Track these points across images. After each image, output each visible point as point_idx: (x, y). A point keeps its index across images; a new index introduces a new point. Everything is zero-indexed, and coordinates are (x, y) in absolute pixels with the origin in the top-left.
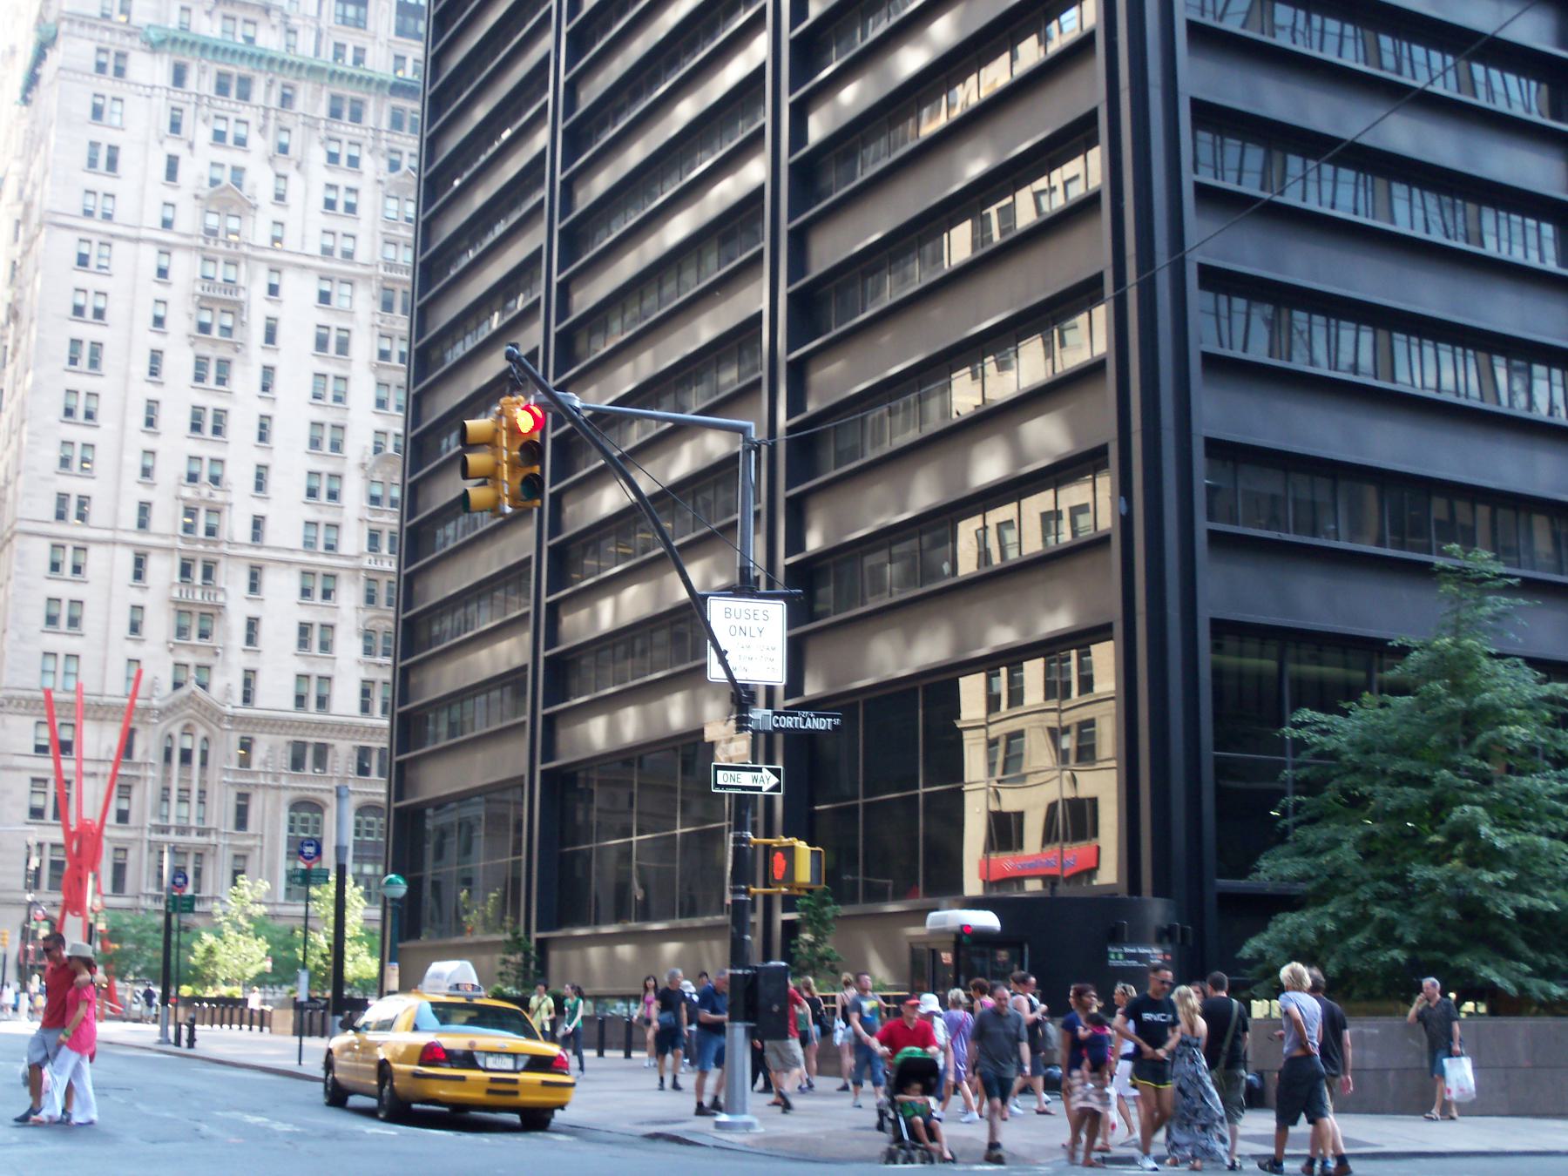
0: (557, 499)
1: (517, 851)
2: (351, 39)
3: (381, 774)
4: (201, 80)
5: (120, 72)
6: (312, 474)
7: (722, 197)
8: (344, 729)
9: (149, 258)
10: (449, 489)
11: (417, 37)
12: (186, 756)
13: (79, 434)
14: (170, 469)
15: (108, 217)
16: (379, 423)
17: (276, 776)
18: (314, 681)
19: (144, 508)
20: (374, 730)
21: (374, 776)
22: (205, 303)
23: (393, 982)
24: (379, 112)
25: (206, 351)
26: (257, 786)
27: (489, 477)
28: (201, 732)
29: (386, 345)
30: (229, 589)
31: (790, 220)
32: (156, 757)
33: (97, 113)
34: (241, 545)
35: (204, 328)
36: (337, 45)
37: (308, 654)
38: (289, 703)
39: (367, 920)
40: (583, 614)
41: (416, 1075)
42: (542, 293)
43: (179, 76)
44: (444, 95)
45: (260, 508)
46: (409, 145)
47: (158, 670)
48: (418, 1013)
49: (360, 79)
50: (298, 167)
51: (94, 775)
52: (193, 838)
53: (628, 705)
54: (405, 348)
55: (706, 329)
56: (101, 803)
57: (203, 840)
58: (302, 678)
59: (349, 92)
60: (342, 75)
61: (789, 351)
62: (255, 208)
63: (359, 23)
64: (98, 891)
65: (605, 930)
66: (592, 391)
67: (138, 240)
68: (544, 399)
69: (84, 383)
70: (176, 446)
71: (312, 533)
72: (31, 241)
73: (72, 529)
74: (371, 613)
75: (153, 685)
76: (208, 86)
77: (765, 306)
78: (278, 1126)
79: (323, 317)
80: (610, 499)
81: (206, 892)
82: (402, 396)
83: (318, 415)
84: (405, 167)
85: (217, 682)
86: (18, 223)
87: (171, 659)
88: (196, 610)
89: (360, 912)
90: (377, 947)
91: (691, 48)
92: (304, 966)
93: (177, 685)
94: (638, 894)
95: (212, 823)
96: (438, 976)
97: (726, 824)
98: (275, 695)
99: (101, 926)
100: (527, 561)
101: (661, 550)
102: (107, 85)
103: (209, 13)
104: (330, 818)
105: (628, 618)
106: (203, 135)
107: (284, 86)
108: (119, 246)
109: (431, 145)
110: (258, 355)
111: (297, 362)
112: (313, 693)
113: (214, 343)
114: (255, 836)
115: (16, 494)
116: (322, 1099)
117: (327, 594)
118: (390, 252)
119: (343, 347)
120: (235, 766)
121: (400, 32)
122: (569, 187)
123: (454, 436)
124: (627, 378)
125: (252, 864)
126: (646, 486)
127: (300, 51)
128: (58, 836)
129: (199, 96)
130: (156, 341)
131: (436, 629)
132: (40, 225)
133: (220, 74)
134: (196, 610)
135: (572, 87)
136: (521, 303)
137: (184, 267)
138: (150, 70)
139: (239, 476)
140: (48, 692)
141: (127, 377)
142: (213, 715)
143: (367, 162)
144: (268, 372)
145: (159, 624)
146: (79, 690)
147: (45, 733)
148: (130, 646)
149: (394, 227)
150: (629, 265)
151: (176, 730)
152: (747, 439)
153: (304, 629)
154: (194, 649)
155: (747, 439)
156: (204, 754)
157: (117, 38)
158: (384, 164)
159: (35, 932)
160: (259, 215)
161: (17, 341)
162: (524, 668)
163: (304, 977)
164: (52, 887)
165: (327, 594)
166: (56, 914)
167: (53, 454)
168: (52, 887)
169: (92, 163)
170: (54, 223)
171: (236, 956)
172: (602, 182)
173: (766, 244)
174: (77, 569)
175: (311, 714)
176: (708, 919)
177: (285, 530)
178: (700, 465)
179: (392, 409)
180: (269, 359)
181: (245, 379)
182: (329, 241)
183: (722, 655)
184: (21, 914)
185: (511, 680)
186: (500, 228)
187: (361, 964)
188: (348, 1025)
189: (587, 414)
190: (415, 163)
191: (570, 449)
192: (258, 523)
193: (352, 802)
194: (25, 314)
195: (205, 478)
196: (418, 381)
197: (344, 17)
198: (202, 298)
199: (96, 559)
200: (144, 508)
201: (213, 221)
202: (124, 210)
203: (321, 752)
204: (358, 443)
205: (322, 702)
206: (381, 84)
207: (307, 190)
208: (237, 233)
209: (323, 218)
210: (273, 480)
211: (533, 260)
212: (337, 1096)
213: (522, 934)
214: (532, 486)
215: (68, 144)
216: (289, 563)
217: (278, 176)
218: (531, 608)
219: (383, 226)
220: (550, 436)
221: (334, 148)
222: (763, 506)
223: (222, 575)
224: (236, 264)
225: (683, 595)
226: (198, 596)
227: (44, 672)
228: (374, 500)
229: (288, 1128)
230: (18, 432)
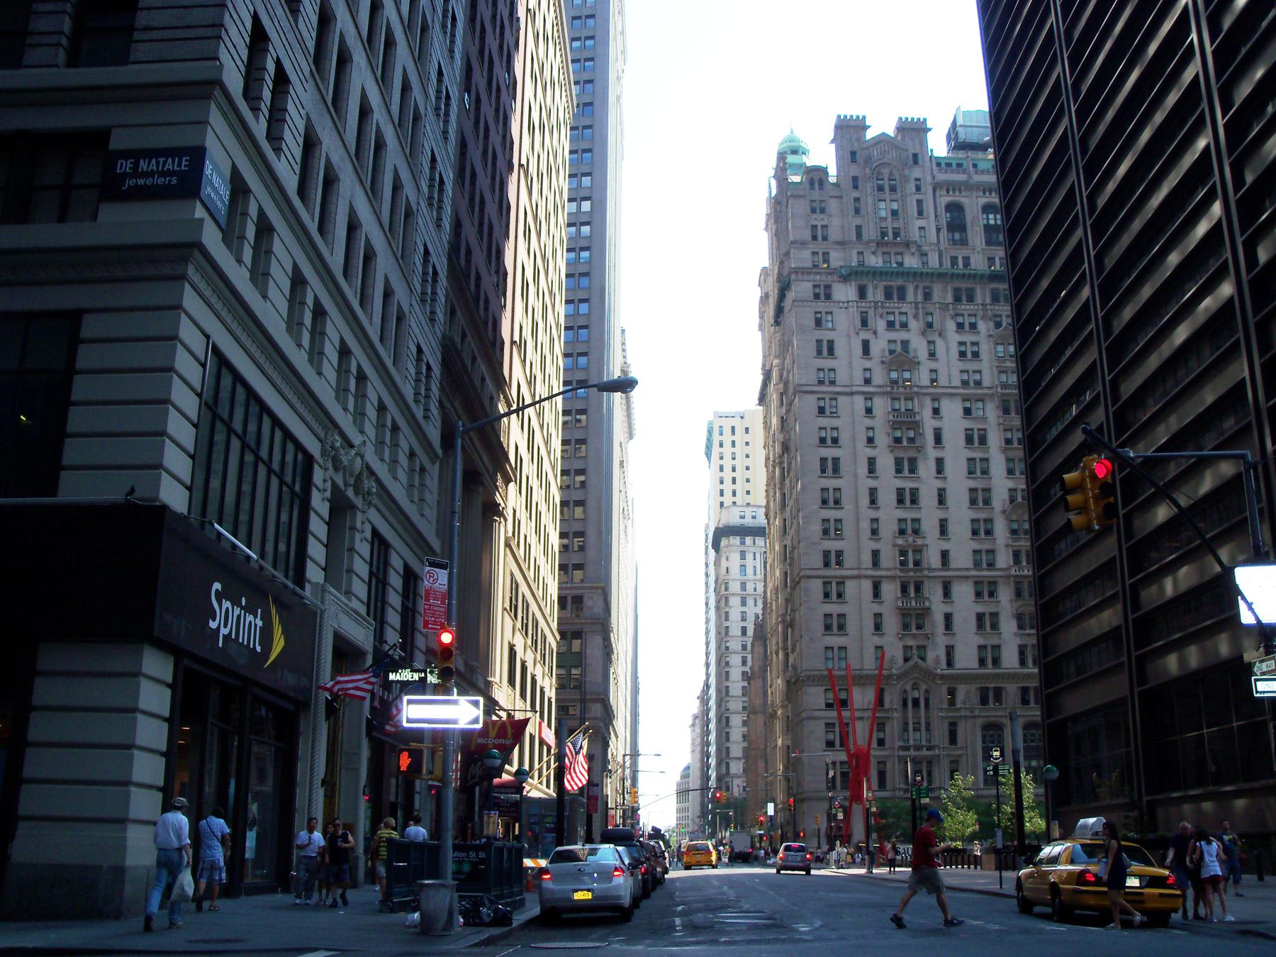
0: (1128, 517)
1: (1128, 744)
2: (960, 253)
3: (1036, 703)
4: (875, 294)
5: (828, 297)
6: (973, 521)
7: (1207, 309)
8: (1012, 677)
9: (859, 402)
10: (1057, 521)
11: (999, 244)
12: (916, 702)
13: (831, 514)
14: (888, 529)
15: (832, 383)
16: (1010, 484)
17: (972, 710)
18: (989, 649)
19: (876, 554)
20: (1029, 676)
21: (1032, 705)
22: (895, 425)
23: (1056, 832)
24: (984, 295)
25: (901, 454)
26: (960, 717)
27: (1083, 509)
28: (923, 687)
29: (1009, 435)
30: (932, 598)
31: (1254, 317)
32: (897, 704)
33: (818, 323)
34: (935, 570)
35: (898, 440)
36: (952, 258)
37: (980, 631)
38: (975, 664)
39: (1036, 796)
40: (1154, 589)
41: (1075, 891)
42: (1100, 388)
43: (862, 293)
44: (1021, 275)
45: (945, 546)
46: (1005, 310)
47: (895, 651)
48: (1073, 852)
49: (969, 275)
50: (940, 335)
51: (861, 718)
52: (925, 752)
53: (1189, 645)
54: (1020, 435)
55: (1209, 396)
56: (867, 735)
57: (931, 753)
58: (982, 648)
59: (963, 285)
60: (958, 275)
61: (1267, 401)
62: (919, 363)
63: (964, 242)
64: (869, 789)
65: (1192, 792)
66: (1141, 446)
67: (852, 394)
68: (1110, 455)
69: (832, 483)
70: (889, 514)
71: (978, 557)
72: (791, 403)
73: (834, 572)
74: (1020, 603)
75: (892, 660)
76: (880, 296)
77: (1246, 373)
78: (991, 926)
79: (968, 424)
80: (1162, 513)
81: (936, 784)
82: (1023, 465)
83: (972, 484)
84: (1004, 324)
85: (931, 655)
86: (782, 394)
87: (901, 644)
88: (913, 613)
89: (1030, 790)
90: (1044, 811)
91: (1171, 220)
92: (999, 826)
93: (906, 660)
94: (1213, 768)
95: (935, 742)
96: (1085, 826)
97: (1268, 717)
98: (967, 659)
99: (874, 809)
100: (1114, 559)
101: (1198, 542)
102: (822, 306)
103: (874, 253)
104: (1007, 733)
105: (1184, 586)
106: (881, 325)
107: (925, 288)
108: (841, 399)
109: (1018, 309)
110: (932, 453)
111: (956, 454)
112: (988, 655)
113: (905, 448)
114: (961, 748)
115: (799, 555)
116: (1016, 909)
117: (991, 594)
118: (1003, 378)
119: (983, 440)
120: (945, 706)
121: (988, 243)
122: (1107, 320)
123: (1058, 486)
124: (1162, 434)
125: (962, 766)
126: (1183, 502)
127: (930, 265)
128: (843, 756)
129: (876, 303)
130: (870, 452)
131: (1061, 608)
132: (794, 394)
133: (886, 288)
134: (913, 613)
135: (1100, 258)
136: (1088, 396)
137: (881, 406)
138: (845, 292)
139: (930, 526)
140: (830, 671)
141: (856, 476)
142: (930, 675)
143: (982, 326)
144: (940, 462)
145: (891, 624)
146: (848, 667)
147: (830, 695)
148: (876, 638)
149: (1004, 362)
150: (1153, 362)
151: (908, 687)
152: (1246, 463)
153: (980, 617)
154: (914, 636)
155: (1246, 463)
156: (927, 700)
157: (824, 277)
158: (991, 324)
159: (835, 815)
160: (921, 368)
161: (789, 464)
162: (1119, 627)
163: (999, 833)
164: (843, 788)
165: (991, 594)
166: (847, 804)
167: (817, 528)
168: (843, 788)
169: (819, 352)
170: (801, 391)
171: (960, 823)
172: (1128, 313)
173: (1241, 335)
174: (840, 595)
175: (990, 670)
176: (1263, 782)
177: (962, 557)
178: (1218, 483)
179: (1018, 474)
180: (939, 454)
181: (926, 469)
182: (965, 377)
183: (1250, 606)
184: (826, 805)
185: (1112, 636)
186: (1068, 352)
187: (1034, 822)
188: (1029, 862)
189: (1139, 460)
190: (1010, 321)
191: (1136, 484)
192: (945, 555)
193: (1020, 722)
194: (792, 446)
195: (909, 531)
196: (1031, 453)
197: (953, 240)
198: (894, 422)
199: (850, 587)
200: (876, 554)
201: (894, 375)
202: (842, 377)
203: (998, 693)
204: (1000, 497)
205: (996, 661)
206: (982, 276)
207: (947, 348)
208: (910, 380)
209: (960, 364)
210: (951, 528)
211: (1091, 369)
212: (1026, 906)
213: (1136, 798)
214: (1109, 512)
215: (803, 346)
216: (966, 577)
217: (929, 342)
218: (1119, 588)
219: (995, 361)
220: (1118, 478)
221: (960, 320)
222: (1264, 504)
223: (926, 591)
224: (912, 399)
225: (1218, 569)
226: (913, 604)
227: (827, 659)
228: (1014, 532)
229: (997, 927)
230: (796, 517)
